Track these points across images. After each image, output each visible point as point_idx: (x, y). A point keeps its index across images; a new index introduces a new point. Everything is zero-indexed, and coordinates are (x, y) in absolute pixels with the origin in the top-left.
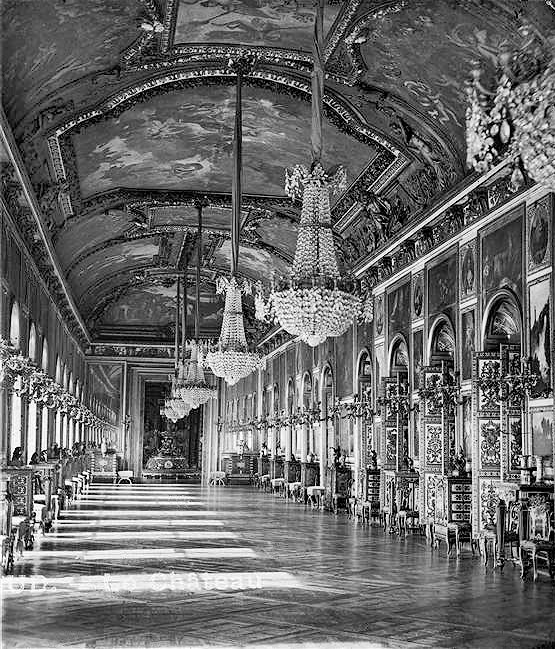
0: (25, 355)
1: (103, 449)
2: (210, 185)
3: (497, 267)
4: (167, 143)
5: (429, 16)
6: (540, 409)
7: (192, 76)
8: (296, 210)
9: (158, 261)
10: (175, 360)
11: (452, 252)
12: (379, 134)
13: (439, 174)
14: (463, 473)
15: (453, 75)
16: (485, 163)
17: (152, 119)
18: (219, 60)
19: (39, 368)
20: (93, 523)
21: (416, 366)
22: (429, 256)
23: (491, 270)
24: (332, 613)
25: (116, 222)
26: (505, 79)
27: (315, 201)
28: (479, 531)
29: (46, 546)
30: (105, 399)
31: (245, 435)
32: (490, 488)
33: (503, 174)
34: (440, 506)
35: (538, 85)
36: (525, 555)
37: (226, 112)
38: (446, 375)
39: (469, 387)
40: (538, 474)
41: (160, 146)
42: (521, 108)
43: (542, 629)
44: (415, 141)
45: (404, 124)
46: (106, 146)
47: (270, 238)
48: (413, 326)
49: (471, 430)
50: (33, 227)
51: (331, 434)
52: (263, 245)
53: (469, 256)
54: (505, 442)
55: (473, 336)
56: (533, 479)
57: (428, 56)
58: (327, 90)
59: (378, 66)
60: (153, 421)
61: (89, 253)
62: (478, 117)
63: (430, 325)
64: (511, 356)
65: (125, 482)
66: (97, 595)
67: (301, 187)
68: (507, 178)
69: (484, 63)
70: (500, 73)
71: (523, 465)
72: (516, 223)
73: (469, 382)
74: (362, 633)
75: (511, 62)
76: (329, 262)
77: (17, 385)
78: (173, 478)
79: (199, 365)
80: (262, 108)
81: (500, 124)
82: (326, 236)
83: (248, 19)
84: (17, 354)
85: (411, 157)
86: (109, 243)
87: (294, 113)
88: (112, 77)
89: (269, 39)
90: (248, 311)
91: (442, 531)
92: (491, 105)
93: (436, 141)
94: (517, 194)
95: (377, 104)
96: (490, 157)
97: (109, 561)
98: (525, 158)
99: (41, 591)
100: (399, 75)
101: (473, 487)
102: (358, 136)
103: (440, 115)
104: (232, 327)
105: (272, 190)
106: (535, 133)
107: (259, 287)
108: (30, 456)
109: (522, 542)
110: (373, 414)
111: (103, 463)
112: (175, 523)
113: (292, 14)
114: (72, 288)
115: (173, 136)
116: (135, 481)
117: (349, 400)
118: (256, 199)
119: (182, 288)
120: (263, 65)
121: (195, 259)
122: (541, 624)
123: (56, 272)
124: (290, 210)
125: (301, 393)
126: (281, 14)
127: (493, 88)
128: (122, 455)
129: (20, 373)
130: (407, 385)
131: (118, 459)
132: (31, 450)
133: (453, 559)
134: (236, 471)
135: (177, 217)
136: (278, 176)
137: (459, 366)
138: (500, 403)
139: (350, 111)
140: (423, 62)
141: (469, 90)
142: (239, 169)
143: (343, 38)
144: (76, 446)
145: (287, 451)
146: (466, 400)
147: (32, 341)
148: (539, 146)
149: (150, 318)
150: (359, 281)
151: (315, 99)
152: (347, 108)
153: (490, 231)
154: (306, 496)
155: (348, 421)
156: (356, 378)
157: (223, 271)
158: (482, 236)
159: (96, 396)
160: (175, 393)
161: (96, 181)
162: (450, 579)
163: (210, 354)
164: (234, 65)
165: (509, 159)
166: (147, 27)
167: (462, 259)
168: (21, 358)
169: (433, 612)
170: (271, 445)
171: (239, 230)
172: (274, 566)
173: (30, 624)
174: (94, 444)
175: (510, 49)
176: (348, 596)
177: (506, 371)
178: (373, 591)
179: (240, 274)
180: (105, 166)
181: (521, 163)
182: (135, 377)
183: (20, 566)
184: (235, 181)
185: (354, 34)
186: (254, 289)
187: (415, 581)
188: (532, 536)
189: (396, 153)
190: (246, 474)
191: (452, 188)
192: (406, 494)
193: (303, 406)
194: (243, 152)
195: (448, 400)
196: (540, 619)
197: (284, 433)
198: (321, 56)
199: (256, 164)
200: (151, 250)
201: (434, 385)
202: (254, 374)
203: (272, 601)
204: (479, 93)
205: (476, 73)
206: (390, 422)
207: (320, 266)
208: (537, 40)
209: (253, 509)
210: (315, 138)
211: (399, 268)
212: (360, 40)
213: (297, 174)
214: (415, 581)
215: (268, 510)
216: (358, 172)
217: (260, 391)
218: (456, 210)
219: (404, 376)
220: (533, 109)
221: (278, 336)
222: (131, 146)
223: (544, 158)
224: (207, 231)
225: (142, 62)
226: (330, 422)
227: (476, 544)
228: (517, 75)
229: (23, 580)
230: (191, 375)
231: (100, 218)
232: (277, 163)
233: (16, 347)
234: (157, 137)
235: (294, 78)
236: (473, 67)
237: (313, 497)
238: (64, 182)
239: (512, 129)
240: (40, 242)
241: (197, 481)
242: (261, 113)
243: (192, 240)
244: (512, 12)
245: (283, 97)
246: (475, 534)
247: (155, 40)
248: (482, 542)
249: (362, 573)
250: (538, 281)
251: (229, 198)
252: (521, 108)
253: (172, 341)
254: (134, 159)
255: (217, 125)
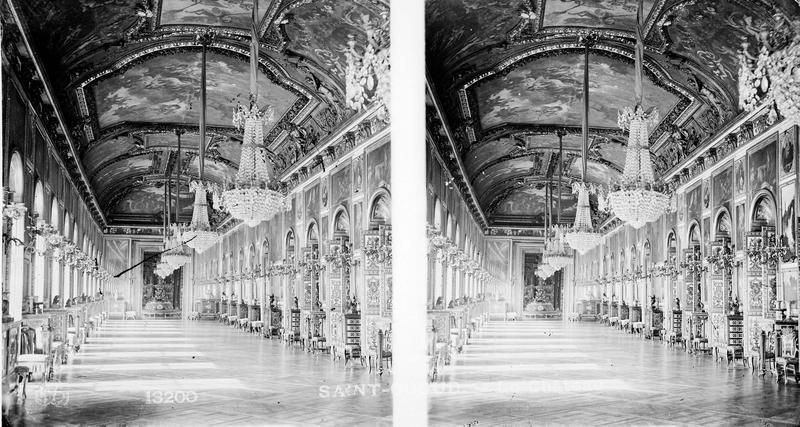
0: (445, 235)
1: (116, 297)
2: (185, 119)
3: (377, 173)
4: (156, 91)
5: (714, 7)
6: (788, 269)
7: (555, 48)
8: (240, 134)
9: (152, 170)
10: (544, 238)
11: (348, 163)
12: (681, 87)
13: (721, 113)
14: (737, 313)
15: (729, 46)
16: (751, 106)
17: (146, 75)
18: (191, 36)
19: (453, 243)
20: (108, 347)
21: (323, 240)
23: (756, 176)
24: (650, 406)
25: (122, 145)
26: (764, 49)
27: (254, 130)
28: (748, 352)
29: (76, 362)
30: (498, 265)
31: (211, 287)
32: (756, 323)
33: (763, 112)
34: (722, 335)
35: (787, 53)
36: (779, 367)
37: (577, 71)
38: (726, 247)
39: (742, 255)
40: (787, 313)
41: (534, 95)
42: (775, 68)
43: (791, 417)
44: (704, 91)
45: (315, 78)
46: (497, 96)
47: (607, 156)
48: (322, 213)
49: (743, 282)
50: (449, 149)
51: (268, 285)
52: (603, 161)
54: (766, 292)
55: (361, 220)
56: (784, 317)
57: (712, 34)
58: (261, 54)
59: (297, 39)
60: (530, 278)
61: (486, 167)
62: (746, 75)
63: (333, 212)
64: (769, 234)
65: (130, 319)
66: (106, 394)
67: (244, 120)
68: (766, 116)
69: (751, 38)
70: (761, 45)
71: (777, 308)
72: (773, 146)
73: (741, 251)
74: (670, 419)
75: (768, 38)
76: (648, 173)
77: (439, 255)
78: (163, 316)
79: (561, 242)
80: (602, 70)
81: (761, 79)
82: (645, 154)
83: (592, 10)
84: (56, 232)
85: (320, 100)
86: (500, 160)
87: (624, 73)
88: (501, 49)
89: (223, 21)
90: (593, 206)
91: (723, 352)
92: (755, 66)
93: (718, 91)
94: (772, 126)
95: (679, 67)
96: (754, 101)
97: (117, 371)
98: (778, 102)
99: (455, 393)
100: (693, 46)
102: (666, 87)
103: (721, 73)
104: (583, 215)
105: (609, 124)
106: (785, 85)
107: (600, 189)
108: (65, 301)
109: (777, 359)
110: (295, 272)
111: (116, 306)
112: (546, 347)
113: (621, 6)
114: (476, 190)
115: (542, 89)
116: (137, 318)
117: (280, 263)
118: (217, 129)
119: (549, 190)
120: (602, 40)
121: (558, 170)
122: (790, 414)
123: (83, 178)
124: (620, 137)
125: (248, 258)
126: (614, 6)
127: (756, 55)
128: (509, 302)
129: (441, 247)
130: (318, 253)
131: (126, 303)
132: (66, 297)
133: (730, 370)
134: (205, 311)
135: (546, 142)
136: (612, 114)
137: (734, 241)
138: (762, 266)
139: (279, 69)
140: (327, 36)
141: (740, 57)
142: (204, 109)
143: (655, 22)
144: (479, 296)
145: (239, 296)
146: (739, 265)
147: (67, 225)
148: (787, 94)
149: (147, 209)
150: (667, 185)
151: (637, 63)
152: (277, 67)
153: (756, 150)
154: (251, 328)
155: (660, 279)
156: (666, 249)
157: (576, 179)
158: (750, 153)
159: (492, 262)
160: (544, 260)
161: (109, 117)
162: (729, 383)
163: (184, 233)
165: (767, 102)
166: (524, 16)
167: (735, 171)
168: (441, 237)
169: (718, 406)
170: (228, 293)
171: (587, 151)
172: (613, 375)
173: (449, 414)
174: (110, 293)
175: (768, 29)
176: (661, 395)
177: (765, 244)
178: (678, 391)
179: (205, 179)
181: (775, 105)
182: (137, 248)
183: (441, 377)
184: (201, 115)
185: (281, 18)
186: (597, 190)
187: (705, 385)
188: (784, 355)
189: (692, 99)
190: (214, 312)
191: (729, 122)
192: (699, 327)
193: (249, 267)
194: (590, 98)
195: (727, 264)
196: (790, 410)
197: (618, 286)
198: (641, 34)
199: (217, 105)
200: (147, 163)
201: (336, 253)
202: (598, 247)
203: (226, 398)
204: (747, 59)
205: (745, 45)
206: (689, 279)
207: (641, 175)
208: (786, 23)
209: (597, 337)
210: (638, 89)
212: (668, 24)
213: (626, 113)
214: (705, 385)
215: (606, 338)
216: (666, 111)
217: (221, 256)
218: (733, 137)
219: (697, 248)
220: (783, 69)
221: (613, 222)
222: (515, 95)
223: (790, 101)
224: (184, 150)
225: (521, 39)
226: (267, 278)
227: (746, 360)
228: (772, 46)
229: (443, 385)
230: (555, 250)
231: (112, 142)
232: (612, 106)
233: (438, 230)
235: (623, 49)
236: (743, 41)
237: (256, 328)
238: (469, 119)
239: (770, 83)
240: (454, 160)
241: (559, 318)
242: (602, 72)
243: (174, 156)
244: (769, 4)
245: (616, 62)
246: (746, 354)
247: (146, 22)
248: (750, 359)
249: (671, 380)
250: (787, 184)
251: (580, 129)
252: (775, 68)
253: (543, 225)
254: (134, 102)
255: (571, 81)
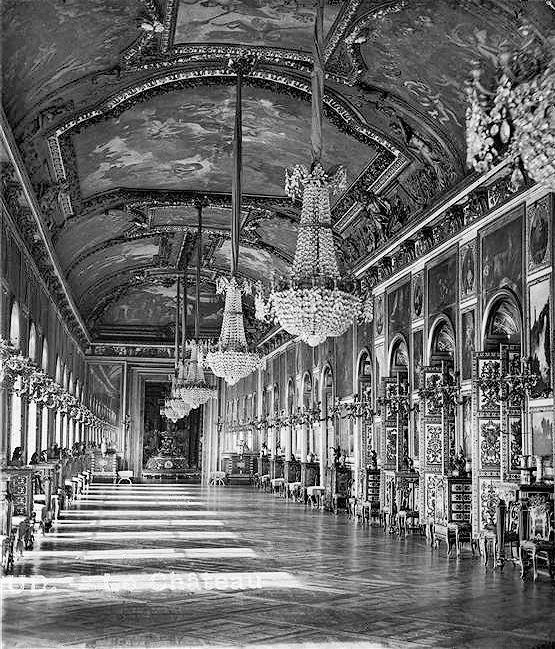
0: (25, 355)
1: (103, 449)
2: (210, 185)
3: (497, 267)
4: (167, 143)
5: (429, 16)
6: (540, 409)
7: (192, 76)
8: (296, 210)
9: (158, 261)
10: (175, 360)
11: (452, 252)
12: (379, 134)
13: (439, 174)
14: (463, 473)
15: (453, 75)
16: (485, 163)
17: (152, 119)
18: (219, 60)
19: (39, 368)
20: (93, 523)
21: (416, 366)
22: (429, 256)
23: (491, 270)
24: (332, 613)
25: (116, 222)
26: (505, 79)
27: (315, 201)
28: (479, 531)
29: (46, 546)
30: (105, 399)
31: (245, 435)
32: (490, 488)
33: (503, 174)
34: (440, 506)
35: (538, 85)
36: (525, 555)
37: (226, 112)
38: (446, 375)
39: (469, 387)
40: (538, 474)
41: (160, 146)
42: (521, 108)
43: (542, 629)
44: (415, 141)
45: (404, 124)
46: (106, 146)
47: (270, 238)
48: (413, 326)
49: (471, 430)
50: (33, 227)
51: (331, 434)
52: (263, 245)
53: (469, 256)
54: (505, 442)
55: (473, 336)
56: (533, 479)
57: (428, 56)
58: (327, 90)
59: (378, 66)
60: (153, 421)
61: (89, 253)
62: (478, 117)
63: (430, 325)
64: (511, 356)
65: (125, 482)
66: (97, 595)
67: (301, 187)
68: (507, 178)
69: (484, 63)
70: (500, 73)
71: (523, 465)
72: (516, 223)
73: (469, 382)
74: (362, 633)
75: (511, 62)
76: (329, 262)
77: (17, 385)
78: (173, 478)
79: (199, 365)
80: (262, 108)
81: (500, 124)
82: (326, 236)
83: (248, 19)
84: (17, 354)
85: (411, 157)
86: (109, 243)
87: (294, 113)
88: (112, 77)
89: (269, 39)
90: (248, 311)
91: (442, 531)
92: (491, 105)
93: (436, 141)
94: (517, 194)
95: (377, 104)
96: (490, 157)
97: (109, 561)
98: (525, 158)
99: (41, 591)
100: (399, 75)
101: (473, 487)
102: (358, 136)
103: (440, 115)
104: (232, 327)
105: (272, 190)
106: (535, 133)
107: (259, 287)
108: (30, 456)
109: (522, 542)
110: (373, 414)
111: (103, 463)
112: (175, 523)
113: (292, 14)
114: (72, 288)
115: (173, 136)
116: (135, 481)
117: (349, 400)
118: (256, 199)
119: (182, 288)
120: (263, 65)
121: (195, 259)
122: (541, 624)
123: (56, 272)
124: (290, 210)
125: (301, 393)
126: (281, 14)
127: (493, 88)
128: (122, 455)
129: (20, 373)
130: (407, 385)
131: (118, 459)
132: (31, 450)
133: (453, 559)
134: (236, 471)
135: (177, 217)
136: (278, 176)
137: (459, 366)
138: (500, 403)
139: (350, 111)
140: (423, 62)
141: (469, 90)
142: (239, 169)
143: (343, 38)
144: (76, 446)
145: (287, 451)
146: (466, 400)
147: (32, 341)
148: (539, 146)
149: (150, 318)
150: (359, 281)
151: (315, 99)
152: (347, 108)
153: (490, 231)
154: (306, 496)
155: (348, 421)
156: (356, 378)
157: (223, 271)
158: (482, 236)
159: (96, 396)
160: (175, 393)
161: (96, 181)
162: (450, 579)
163: (210, 354)
164: (234, 65)
165: (509, 159)
166: (147, 27)
167: (462, 259)
168: (21, 358)
169: (433, 612)
170: (271, 445)
171: (239, 230)
172: (274, 566)
173: (30, 624)
174: (94, 444)
175: (510, 49)
176: (348, 596)
177: (506, 371)
178: (373, 591)
179: (240, 274)
180: (105, 166)
181: (521, 163)
182: (135, 377)
183: (20, 566)
184: (235, 181)
185: (354, 34)
186: (254, 289)
187: (415, 581)
188: (532, 536)
189: (396, 153)
190: (246, 474)
191: (452, 188)
192: (406, 494)
193: (303, 406)
194: (243, 152)
195: (448, 400)
196: (540, 619)
197: (284, 433)
198: (321, 56)
199: (256, 164)
200: (151, 250)
201: (434, 385)
202: (254, 374)
203: (272, 601)
204: (479, 93)
205: (476, 73)
206: (390, 422)
207: (320, 266)
208: (537, 40)
209: (253, 509)
210: (315, 138)
211: (399, 268)
212: (360, 40)
213: (297, 174)
214: (415, 581)
215: (268, 510)
216: (358, 172)
217: (260, 391)
218: (456, 210)
219: (404, 376)
220: (533, 109)
221: (278, 336)
222: (131, 146)
223: (544, 158)
224: (207, 231)
225: (142, 62)
226: (330, 422)
227: (476, 544)
228: (517, 75)
229: (23, 580)
230: (191, 375)
231: (100, 218)
232: (277, 163)
233: (16, 347)
234: (157, 137)
235: (294, 78)
236: (473, 67)
237: (313, 497)
238: (64, 182)
239: (512, 129)
240: (40, 242)
241: (197, 481)
242: (261, 113)
243: (192, 240)
244: (512, 12)
245: (283, 97)
246: (475, 534)
247: (155, 40)
248: (482, 542)
249: (362, 573)
250: (538, 281)
251: (229, 198)
252: (521, 108)
253: (172, 341)
254: (134, 159)
255: (217, 125)
